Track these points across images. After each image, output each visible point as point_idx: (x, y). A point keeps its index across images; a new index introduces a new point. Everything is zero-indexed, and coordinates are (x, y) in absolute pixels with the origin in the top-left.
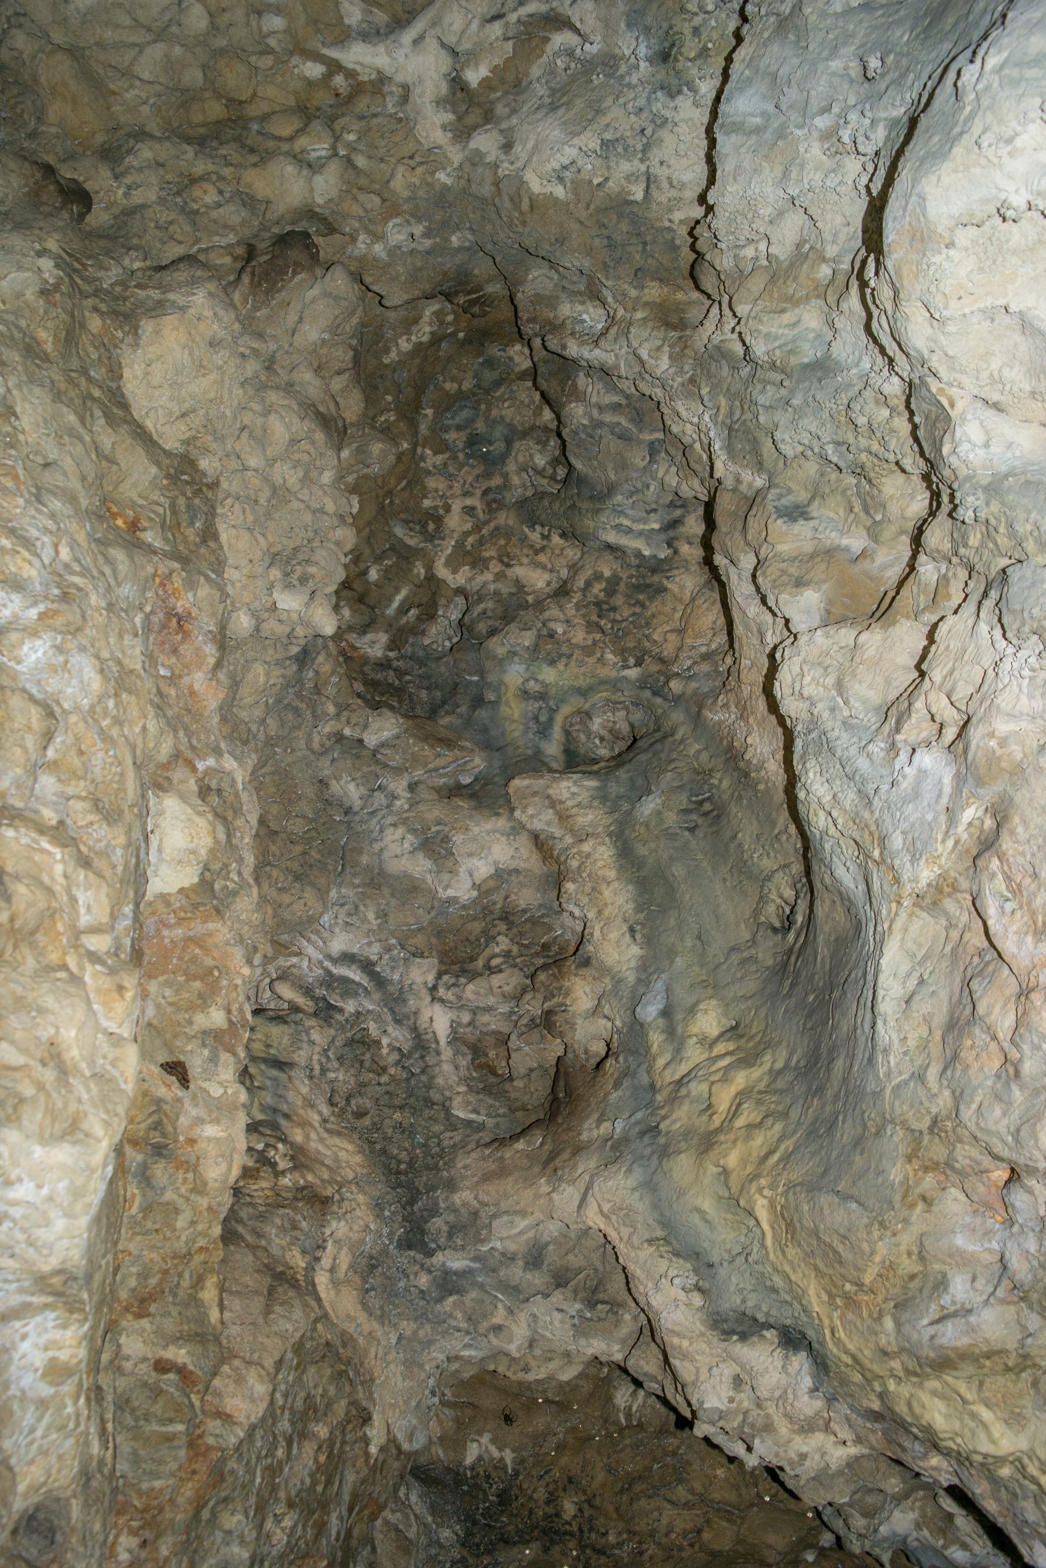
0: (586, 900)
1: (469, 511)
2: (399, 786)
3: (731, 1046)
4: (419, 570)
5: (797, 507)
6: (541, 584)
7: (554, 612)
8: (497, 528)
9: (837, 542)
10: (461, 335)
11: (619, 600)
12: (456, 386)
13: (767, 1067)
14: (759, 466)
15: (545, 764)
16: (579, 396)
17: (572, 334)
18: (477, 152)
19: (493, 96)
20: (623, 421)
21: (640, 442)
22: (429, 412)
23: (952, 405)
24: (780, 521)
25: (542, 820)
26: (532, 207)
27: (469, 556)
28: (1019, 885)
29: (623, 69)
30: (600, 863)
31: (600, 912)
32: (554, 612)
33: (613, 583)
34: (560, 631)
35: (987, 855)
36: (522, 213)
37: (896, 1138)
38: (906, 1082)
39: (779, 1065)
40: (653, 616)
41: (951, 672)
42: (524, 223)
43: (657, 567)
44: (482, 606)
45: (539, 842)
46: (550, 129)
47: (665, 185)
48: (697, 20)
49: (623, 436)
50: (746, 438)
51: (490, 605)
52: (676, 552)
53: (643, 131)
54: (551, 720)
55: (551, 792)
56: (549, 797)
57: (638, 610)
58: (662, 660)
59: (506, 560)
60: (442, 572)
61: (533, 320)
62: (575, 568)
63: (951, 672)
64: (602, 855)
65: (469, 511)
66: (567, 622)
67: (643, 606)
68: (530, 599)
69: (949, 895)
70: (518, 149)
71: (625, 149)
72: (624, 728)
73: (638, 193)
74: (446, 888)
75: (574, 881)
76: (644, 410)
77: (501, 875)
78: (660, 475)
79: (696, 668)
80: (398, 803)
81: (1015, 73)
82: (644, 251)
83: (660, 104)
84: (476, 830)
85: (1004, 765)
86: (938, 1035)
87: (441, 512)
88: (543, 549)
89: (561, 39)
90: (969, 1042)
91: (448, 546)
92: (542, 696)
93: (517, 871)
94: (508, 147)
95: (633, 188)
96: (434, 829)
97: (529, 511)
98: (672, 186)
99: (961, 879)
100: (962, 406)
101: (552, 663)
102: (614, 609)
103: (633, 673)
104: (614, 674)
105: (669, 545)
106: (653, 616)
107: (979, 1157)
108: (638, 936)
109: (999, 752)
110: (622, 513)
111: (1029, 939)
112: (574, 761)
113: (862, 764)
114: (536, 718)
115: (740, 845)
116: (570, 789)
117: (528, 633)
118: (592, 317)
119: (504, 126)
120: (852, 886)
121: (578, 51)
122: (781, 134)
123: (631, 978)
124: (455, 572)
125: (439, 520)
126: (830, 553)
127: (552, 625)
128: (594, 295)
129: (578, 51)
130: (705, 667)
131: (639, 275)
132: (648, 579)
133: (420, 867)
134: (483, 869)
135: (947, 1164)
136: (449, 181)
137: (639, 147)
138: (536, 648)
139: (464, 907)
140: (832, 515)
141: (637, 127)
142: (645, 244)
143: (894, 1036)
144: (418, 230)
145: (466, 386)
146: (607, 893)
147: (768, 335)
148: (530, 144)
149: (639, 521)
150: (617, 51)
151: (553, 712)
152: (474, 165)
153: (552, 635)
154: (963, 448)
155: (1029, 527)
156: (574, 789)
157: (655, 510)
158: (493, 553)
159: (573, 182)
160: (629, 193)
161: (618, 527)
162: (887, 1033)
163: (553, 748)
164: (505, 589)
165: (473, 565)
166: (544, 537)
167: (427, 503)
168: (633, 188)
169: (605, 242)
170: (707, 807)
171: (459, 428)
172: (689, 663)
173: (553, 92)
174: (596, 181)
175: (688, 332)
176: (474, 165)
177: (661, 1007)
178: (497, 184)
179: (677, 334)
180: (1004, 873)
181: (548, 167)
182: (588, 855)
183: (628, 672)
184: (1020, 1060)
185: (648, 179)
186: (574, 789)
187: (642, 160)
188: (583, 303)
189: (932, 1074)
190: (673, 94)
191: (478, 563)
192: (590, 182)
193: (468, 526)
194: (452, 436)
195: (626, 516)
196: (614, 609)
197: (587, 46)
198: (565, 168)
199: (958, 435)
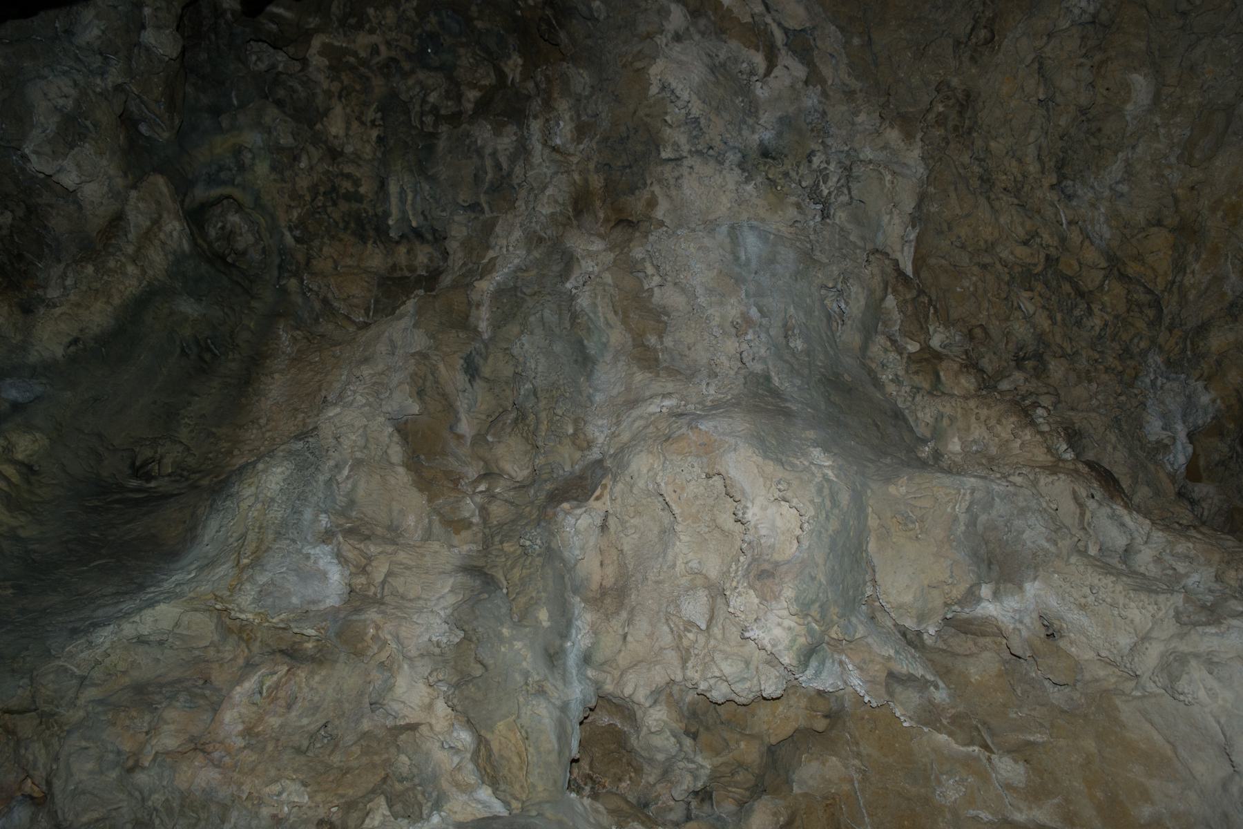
0: (84, 288)
2: (115, 76)
3: (15, 478)
4: (313, 22)
5: (477, 369)
6: (334, 131)
7: (316, 154)
8: (368, 79)
9: (461, 410)
10: (519, 13)
11: (344, 206)
12: (476, 15)
13: (14, 523)
14: (496, 326)
15: (185, 195)
16: (497, 132)
17: (547, 120)
18: (669, 12)
19: (710, 13)
20: (490, 176)
23: (598, 499)
24: (462, 361)
25: (137, 218)
26: (638, 70)
27: (337, 61)
28: (277, 699)
29: (751, 121)
30: (121, 287)
31: (78, 305)
32: (316, 154)
33: (359, 198)
34: (302, 165)
35: (287, 659)
36: (631, 63)
37: (20, 691)
38: (73, 675)
39: (23, 533)
40: (341, 240)
41: (408, 568)
42: (624, 66)
43: (381, 232)
44: (299, 88)
45: (117, 221)
46: (698, 72)
47: (676, 174)
48: (793, 174)
49: (477, 179)
50: (511, 301)
52: (398, 243)
53: (711, 148)
54: (224, 183)
55: (165, 215)
56: (160, 216)
57: (341, 225)
58: (308, 263)
59: (344, 94)
60: (317, 42)
61: (549, 80)
62: (357, 159)
63: (408, 568)
65: (375, 50)
67: (345, 229)
68: (318, 126)
69: (241, 638)
70: (678, 47)
71: (695, 137)
72: (241, 244)
74: (35, 152)
75: (97, 271)
76: (502, 190)
77: (70, 194)
78: (456, 218)
79: (313, 297)
80: (98, 81)
81: (826, 491)
82: (625, 167)
83: (733, 157)
84: (104, 163)
85: (360, 646)
86: (126, 680)
87: (367, 26)
88: (363, 123)
89: (759, 60)
90: (135, 714)
91: (339, 42)
92: (242, 168)
93: (80, 208)
95: (669, 149)
96: (88, 123)
97: (391, 105)
98: (677, 179)
99: (258, 644)
100: (598, 506)
101: (273, 168)
102: (335, 204)
103: (289, 239)
104: (283, 224)
105: (402, 237)
106: (341, 240)
107: (40, 765)
108: (72, 349)
109: (368, 638)
110: (415, 192)
111: (240, 727)
112: (196, 217)
113: (308, 514)
115: (189, 403)
116: (174, 227)
117: (291, 140)
118: (564, 132)
120: (206, 539)
121: (756, 78)
122: (739, 281)
123: (33, 358)
124: (321, 53)
125: (359, 26)
126: (450, 408)
128: (581, 131)
129: (756, 78)
130: (317, 306)
131: (605, 167)
132: (369, 227)
133: (45, 122)
134: (69, 179)
135: (18, 742)
137: (700, 147)
138: (280, 149)
139: (23, 170)
140: (480, 398)
141: (714, 144)
142: (630, 167)
143: (107, 645)
145: (479, 24)
146: (99, 305)
147: (595, 305)
148: (683, 58)
149: (414, 208)
150: (761, 112)
151: (231, 182)
152: (659, 12)
153: (296, 158)
154: (571, 520)
155: (534, 594)
156: (175, 234)
157: (426, 218)
158: (346, 82)
159: (663, 99)
160: (665, 147)
161: (402, 191)
162: (104, 636)
163: (201, 193)
164: (320, 100)
165: (331, 68)
166: (373, 122)
167: (371, 11)
168: (669, 149)
170: (207, 357)
172: (315, 288)
173: (723, 65)
174: (668, 118)
175: (575, 223)
176: (659, 12)
177: (20, 400)
178: (650, 36)
179: (571, 214)
180: (280, 679)
181: (671, 80)
182: (125, 274)
183: (287, 234)
184: (143, 768)
186: (175, 234)
187: (690, 151)
188: (571, 118)
189: (91, 693)
190: (741, 166)
191: (335, 69)
192: (666, 113)
193: (363, 54)
194: (433, 19)
195: (415, 197)
196: (335, 204)
197: (759, 84)
198: (673, 91)
199: (578, 511)
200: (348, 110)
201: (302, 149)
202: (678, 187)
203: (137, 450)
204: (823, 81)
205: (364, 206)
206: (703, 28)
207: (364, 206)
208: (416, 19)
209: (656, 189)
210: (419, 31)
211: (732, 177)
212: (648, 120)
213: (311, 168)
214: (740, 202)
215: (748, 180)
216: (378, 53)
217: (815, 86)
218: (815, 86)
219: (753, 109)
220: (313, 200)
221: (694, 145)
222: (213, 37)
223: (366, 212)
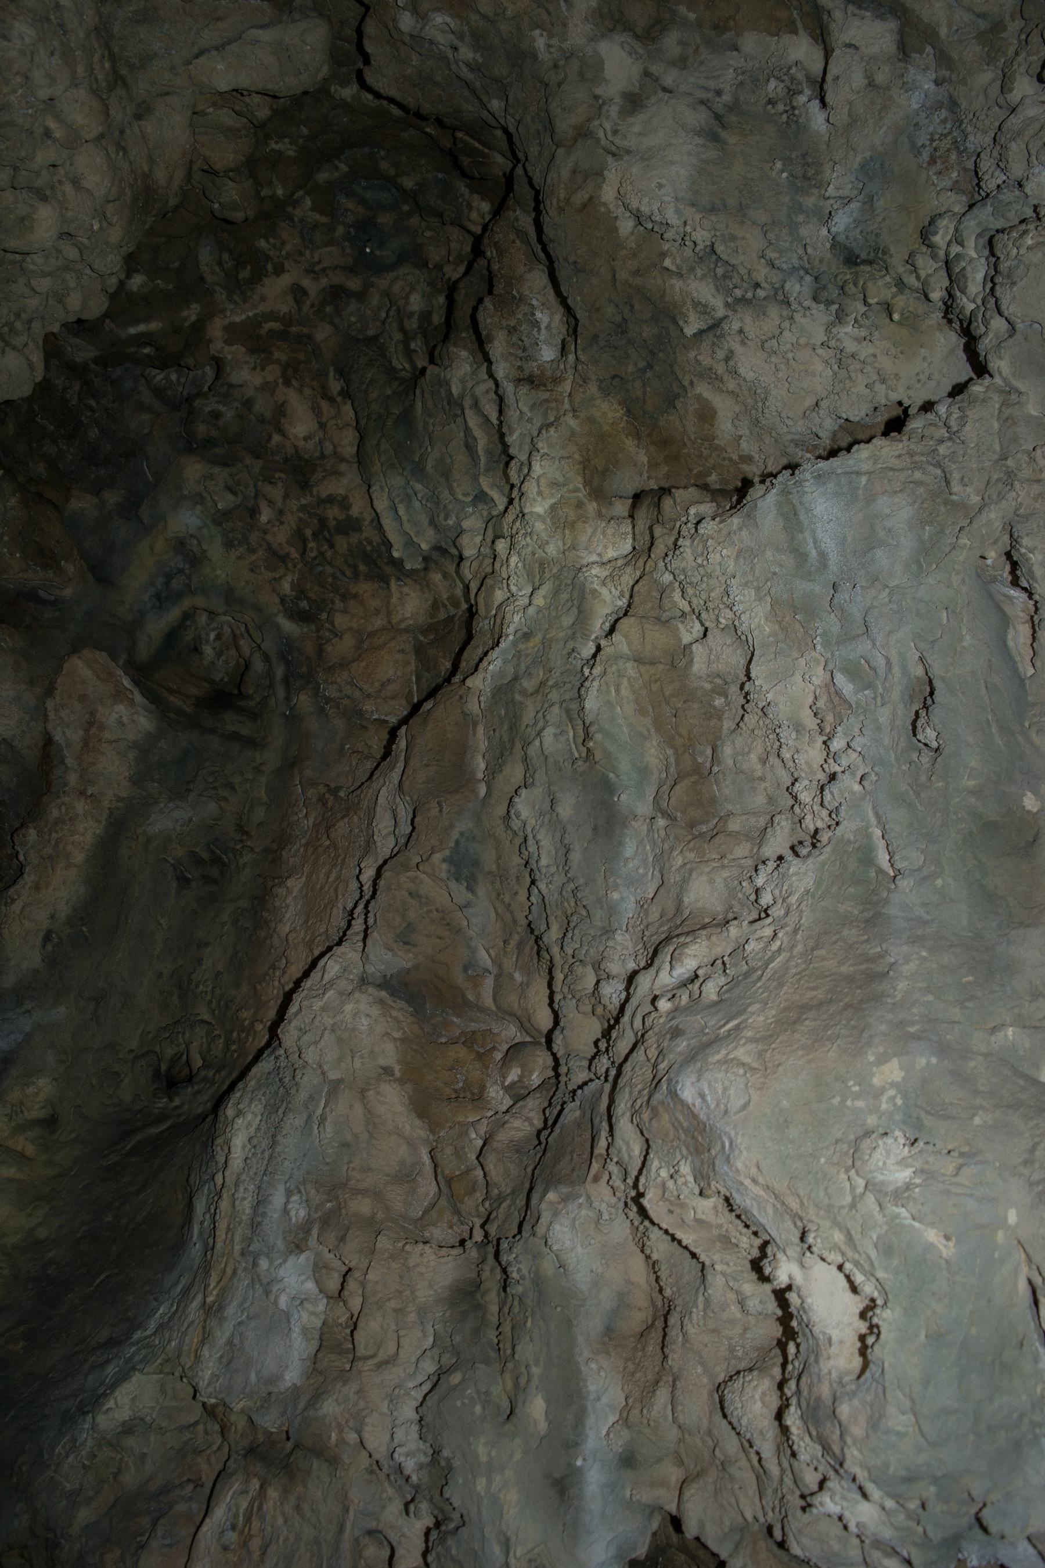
1: (298, 292)
4: (191, 313)
11: (342, 543)
21: (476, 479)
22: (343, 168)
26: (584, 206)
29: (809, 201)
34: (264, 518)
36: (568, 201)
47: (721, 354)
51: (229, 414)
53: (757, 285)
56: (93, 713)
58: (320, 650)
60: (216, 330)
64: (84, 832)
65: (298, 292)
66: (278, 516)
70: (637, 123)
71: (725, 277)
73: (692, 326)
82: (643, 371)
83: (798, 288)
87: (270, 267)
94: (634, 102)
95: (692, 317)
98: (727, 359)
108: (49, 947)
114: (169, 577)
117: (230, 497)
119: (655, 69)
124: (229, 342)
125: (257, 278)
127: (263, 505)
136: (543, 55)
137: (738, 293)
144: (466, 53)
153: (254, 512)
168: (692, 317)
169: (619, 319)
171: (363, 202)
174: (667, 263)
178: (583, 133)
185: (711, 328)
200: (307, 391)
201: (256, 496)
202: (735, 373)
203: (157, 1049)
204: (930, 35)
205: (365, 535)
206: (677, 51)
207: (365, 535)
208: (324, 220)
209: (703, 389)
210: (340, 231)
211: (814, 322)
212: (638, 281)
213: (281, 512)
214: (842, 359)
215: (840, 317)
216: (304, 292)
217: (921, 51)
218: (921, 51)
219: (807, 172)
220: (303, 553)
221: (729, 292)
222: (92, 403)
223: (370, 543)
